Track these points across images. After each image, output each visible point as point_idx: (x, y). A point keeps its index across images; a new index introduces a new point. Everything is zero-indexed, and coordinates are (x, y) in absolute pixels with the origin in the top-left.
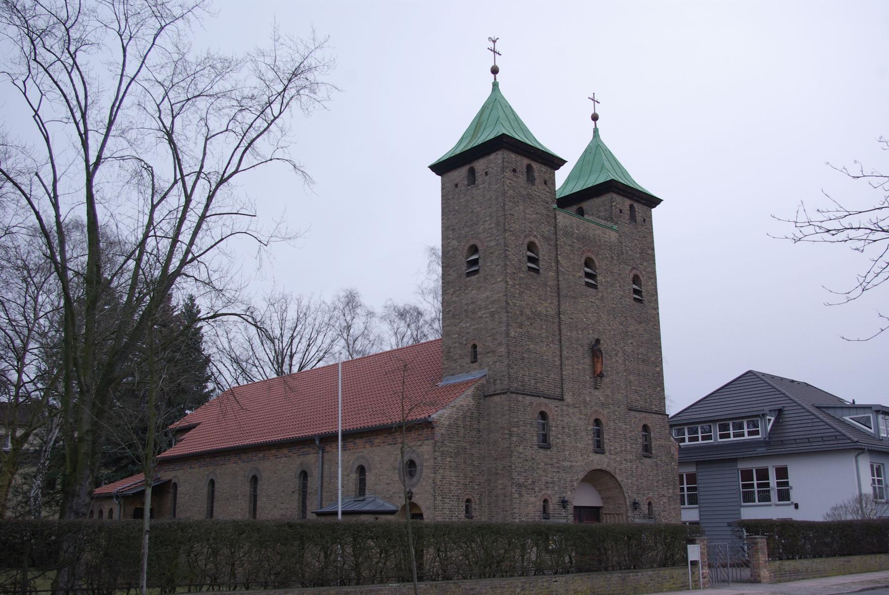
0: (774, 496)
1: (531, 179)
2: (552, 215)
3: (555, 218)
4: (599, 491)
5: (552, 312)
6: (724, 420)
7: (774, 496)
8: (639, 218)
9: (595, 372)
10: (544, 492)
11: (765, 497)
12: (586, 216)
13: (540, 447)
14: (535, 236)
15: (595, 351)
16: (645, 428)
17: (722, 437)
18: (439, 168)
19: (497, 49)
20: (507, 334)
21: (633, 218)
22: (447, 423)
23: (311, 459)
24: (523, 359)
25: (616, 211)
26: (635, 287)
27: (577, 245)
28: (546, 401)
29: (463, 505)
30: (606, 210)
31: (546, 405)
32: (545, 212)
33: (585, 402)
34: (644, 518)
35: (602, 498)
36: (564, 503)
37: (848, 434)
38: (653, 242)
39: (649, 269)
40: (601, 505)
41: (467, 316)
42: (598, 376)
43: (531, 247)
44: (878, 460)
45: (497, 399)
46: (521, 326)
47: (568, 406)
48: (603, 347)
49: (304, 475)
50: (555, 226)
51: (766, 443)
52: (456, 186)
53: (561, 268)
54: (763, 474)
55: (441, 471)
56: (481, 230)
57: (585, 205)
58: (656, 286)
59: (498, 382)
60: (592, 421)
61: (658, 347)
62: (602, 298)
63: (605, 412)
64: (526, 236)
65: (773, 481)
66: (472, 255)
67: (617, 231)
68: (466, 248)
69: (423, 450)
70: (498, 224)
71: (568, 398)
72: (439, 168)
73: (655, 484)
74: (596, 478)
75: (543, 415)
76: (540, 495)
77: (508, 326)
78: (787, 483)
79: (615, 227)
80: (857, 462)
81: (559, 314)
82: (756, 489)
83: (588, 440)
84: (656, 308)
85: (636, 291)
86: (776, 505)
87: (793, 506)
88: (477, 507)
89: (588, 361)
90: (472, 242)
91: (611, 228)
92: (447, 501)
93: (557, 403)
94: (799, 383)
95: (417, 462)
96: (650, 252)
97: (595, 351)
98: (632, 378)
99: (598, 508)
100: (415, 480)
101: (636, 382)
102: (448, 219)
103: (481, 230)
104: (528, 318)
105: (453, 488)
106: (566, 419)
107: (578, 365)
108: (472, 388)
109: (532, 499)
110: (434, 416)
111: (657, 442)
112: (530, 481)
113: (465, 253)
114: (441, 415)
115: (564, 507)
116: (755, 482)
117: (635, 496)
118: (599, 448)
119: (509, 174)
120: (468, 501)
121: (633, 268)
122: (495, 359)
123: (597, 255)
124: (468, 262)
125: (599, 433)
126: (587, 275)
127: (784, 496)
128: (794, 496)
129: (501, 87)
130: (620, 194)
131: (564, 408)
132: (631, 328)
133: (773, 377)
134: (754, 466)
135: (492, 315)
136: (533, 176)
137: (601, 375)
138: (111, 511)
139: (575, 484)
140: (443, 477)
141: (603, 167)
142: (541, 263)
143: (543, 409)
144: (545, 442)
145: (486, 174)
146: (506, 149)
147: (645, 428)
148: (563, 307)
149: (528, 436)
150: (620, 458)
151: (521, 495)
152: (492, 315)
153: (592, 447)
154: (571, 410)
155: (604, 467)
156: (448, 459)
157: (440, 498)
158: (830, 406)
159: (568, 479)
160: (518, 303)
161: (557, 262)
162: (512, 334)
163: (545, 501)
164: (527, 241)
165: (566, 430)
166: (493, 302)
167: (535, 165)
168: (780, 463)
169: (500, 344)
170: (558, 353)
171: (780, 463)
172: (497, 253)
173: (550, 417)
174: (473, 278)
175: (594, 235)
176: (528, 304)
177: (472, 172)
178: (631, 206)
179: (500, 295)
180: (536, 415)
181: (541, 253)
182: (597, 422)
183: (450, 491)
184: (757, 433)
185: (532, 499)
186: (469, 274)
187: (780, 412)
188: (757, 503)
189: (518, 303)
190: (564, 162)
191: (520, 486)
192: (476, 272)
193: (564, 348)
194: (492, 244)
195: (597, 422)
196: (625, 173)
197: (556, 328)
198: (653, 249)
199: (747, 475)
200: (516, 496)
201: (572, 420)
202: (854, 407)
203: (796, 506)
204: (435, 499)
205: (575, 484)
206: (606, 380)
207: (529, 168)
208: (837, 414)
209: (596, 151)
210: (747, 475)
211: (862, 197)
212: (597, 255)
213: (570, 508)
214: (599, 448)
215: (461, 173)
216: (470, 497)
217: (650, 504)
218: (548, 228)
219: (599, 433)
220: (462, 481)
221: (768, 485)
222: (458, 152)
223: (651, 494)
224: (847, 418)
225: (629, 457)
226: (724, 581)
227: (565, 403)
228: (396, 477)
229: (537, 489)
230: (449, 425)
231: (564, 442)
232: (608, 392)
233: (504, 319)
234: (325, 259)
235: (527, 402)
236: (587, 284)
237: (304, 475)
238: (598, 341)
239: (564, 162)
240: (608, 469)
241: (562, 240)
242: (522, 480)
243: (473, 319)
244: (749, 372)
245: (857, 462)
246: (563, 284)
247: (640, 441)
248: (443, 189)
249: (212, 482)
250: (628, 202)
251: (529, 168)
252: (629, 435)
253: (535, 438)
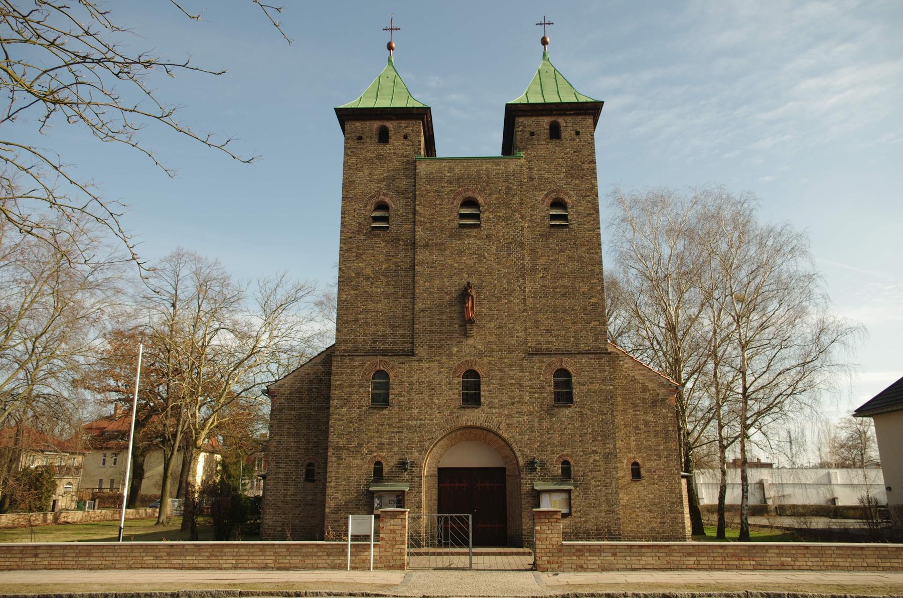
10: (375, 454)
31: (386, 363)
62: (488, 237)
81: (414, 265)
98: (540, 316)
105: (290, 453)
111: (585, 389)
115: (635, 464)
120: (310, 465)
130: (526, 116)
151: (339, 458)
156: (286, 426)
159: (417, 439)
165: (416, 387)
170: (411, 307)
175: (478, 172)
190: (336, 109)
191: (339, 448)
216: (313, 461)
230: (291, 394)
239: (336, 109)
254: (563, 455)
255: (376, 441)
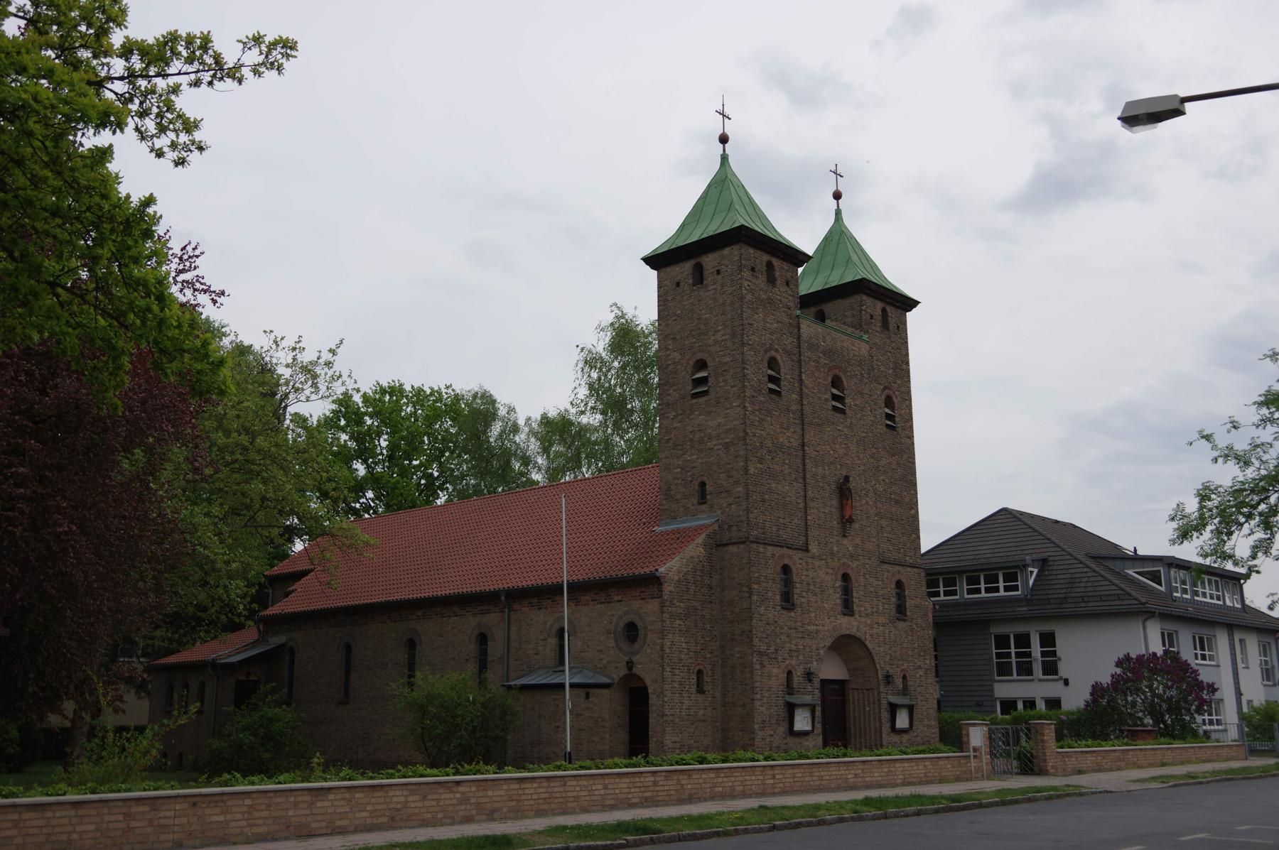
0: (1038, 669)
1: (771, 280)
2: (795, 323)
3: (799, 327)
4: (846, 662)
5: (795, 444)
6: (972, 571)
7: (1038, 669)
8: (892, 326)
9: (843, 516)
11: (1026, 669)
12: (828, 322)
13: (783, 608)
14: (777, 351)
15: (844, 491)
16: (899, 584)
17: (969, 592)
18: (653, 261)
19: (727, 112)
20: (746, 471)
21: (885, 325)
23: (493, 620)
24: (764, 501)
25: (865, 317)
26: (835, 391)
27: (823, 361)
28: (790, 552)
29: (694, 676)
30: (854, 316)
31: (790, 557)
32: (786, 320)
34: (898, 694)
35: (849, 670)
36: (809, 676)
37: (1133, 593)
38: (907, 355)
39: (903, 389)
40: (847, 678)
41: (692, 447)
42: (846, 522)
43: (773, 363)
44: (1170, 627)
45: (733, 549)
46: (761, 461)
47: (813, 558)
48: (852, 485)
49: (483, 639)
50: (799, 337)
51: (1027, 601)
52: (678, 284)
53: (805, 390)
54: (1023, 641)
56: (711, 341)
57: (828, 307)
58: (910, 409)
59: (735, 528)
60: (839, 576)
61: (912, 485)
63: (855, 564)
64: (766, 351)
65: (1036, 649)
66: (698, 371)
67: (867, 342)
68: (692, 363)
69: (645, 609)
70: (733, 335)
71: (814, 548)
72: (653, 261)
73: (910, 653)
74: (845, 646)
75: (786, 569)
76: (783, 665)
77: (746, 461)
78: (1054, 653)
79: (865, 337)
80: (1144, 628)
81: (803, 445)
82: (1014, 660)
83: (836, 598)
84: (911, 437)
85: (889, 417)
86: (1040, 680)
87: (1062, 683)
89: (835, 502)
90: (699, 356)
91: (860, 338)
92: (677, 672)
93: (801, 554)
94: (1064, 524)
95: (640, 625)
96: (904, 367)
97: (844, 491)
98: (884, 523)
99: (841, 683)
100: (637, 646)
101: (889, 529)
102: (667, 325)
103: (711, 341)
104: (770, 451)
106: (811, 574)
107: (824, 508)
108: (703, 536)
109: (775, 671)
110: (662, 570)
112: (772, 649)
113: (690, 369)
114: (671, 568)
115: (810, 681)
116: (1013, 650)
117: (888, 668)
118: (848, 607)
119: (746, 274)
121: (886, 388)
122: (731, 500)
123: (845, 373)
124: (694, 380)
125: (847, 591)
126: (835, 397)
127: (1051, 668)
128: (1064, 670)
129: (732, 161)
131: (810, 560)
132: (882, 463)
133: (1032, 516)
134: (1012, 630)
135: (726, 446)
136: (774, 276)
137: (851, 520)
138: (203, 684)
139: (822, 652)
140: (673, 644)
141: (849, 260)
142: (783, 383)
143: (786, 562)
144: (788, 600)
145: (718, 272)
146: (745, 243)
147: (899, 584)
148: (807, 436)
149: (770, 594)
150: (869, 623)
152: (726, 446)
153: (839, 608)
154: (817, 563)
155: (854, 632)
157: (668, 669)
158: (1108, 556)
160: (759, 432)
161: (801, 382)
162: (752, 471)
163: (789, 673)
164: (767, 357)
166: (727, 431)
167: (776, 262)
168: (1046, 627)
169: (737, 482)
171: (1046, 627)
172: (732, 371)
173: (794, 571)
174: (702, 400)
176: (768, 434)
177: (699, 269)
178: (884, 310)
179: (737, 422)
180: (779, 569)
181: (782, 371)
182: (846, 577)
183: (680, 660)
184: (1016, 588)
186: (695, 396)
187: (1043, 563)
188: (1015, 676)
189: (759, 432)
191: (761, 654)
192: (705, 393)
193: (809, 487)
194: (727, 359)
195: (846, 577)
196: (874, 267)
197: (799, 461)
198: (908, 363)
199: (1002, 641)
200: (758, 666)
201: (817, 575)
202: (1136, 559)
203: (1066, 682)
204: (663, 670)
205: (822, 652)
206: (856, 526)
207: (769, 264)
208: (1117, 566)
209: (838, 238)
210: (1002, 641)
211: (1262, 399)
212: (845, 373)
213: (817, 683)
214: (848, 607)
215: (683, 270)
217: (904, 677)
218: (790, 340)
219: (847, 591)
221: (1029, 655)
222: (680, 243)
223: (905, 666)
224: (1130, 572)
225: (882, 619)
226: (1005, 772)
228: (612, 643)
230: (678, 581)
232: (858, 541)
233: (742, 453)
235: (769, 554)
236: (835, 408)
237: (483, 639)
238: (847, 478)
240: (858, 634)
241: (807, 354)
242: (763, 648)
243: (700, 451)
244: (1004, 512)
245: (1144, 628)
246: (807, 409)
247: (894, 600)
248: (659, 287)
249: (348, 648)
250: (880, 305)
251: (769, 264)
252: (881, 593)
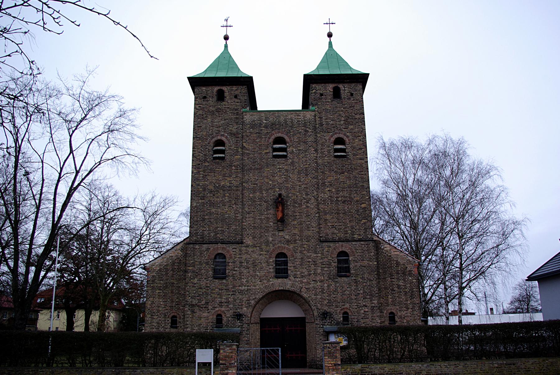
10: (217, 309)
22: (158, 268)
28: (224, 246)
33: (268, 241)
55: (151, 299)
62: (292, 163)
71: (248, 241)
73: (353, 297)
88: (181, 321)
112: (203, 302)
144: (220, 274)
151: (193, 312)
154: (250, 250)
155: (288, 287)
156: (157, 291)
159: (245, 299)
173: (228, 256)
175: (285, 120)
176: (211, 183)
183: (158, 311)
185: (205, 314)
190: (368, 74)
220: (169, 304)
227: (245, 245)
229: (210, 307)
230: (160, 270)
231: (240, 273)
232: (296, 231)
234: (146, 181)
242: (195, 302)
253: (211, 272)
254: (344, 308)
255: (218, 300)
